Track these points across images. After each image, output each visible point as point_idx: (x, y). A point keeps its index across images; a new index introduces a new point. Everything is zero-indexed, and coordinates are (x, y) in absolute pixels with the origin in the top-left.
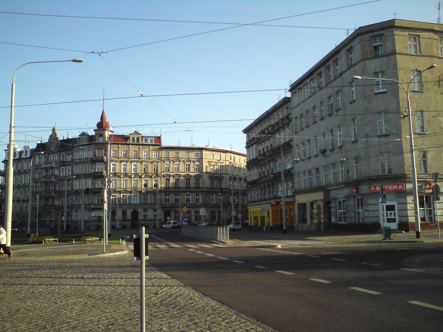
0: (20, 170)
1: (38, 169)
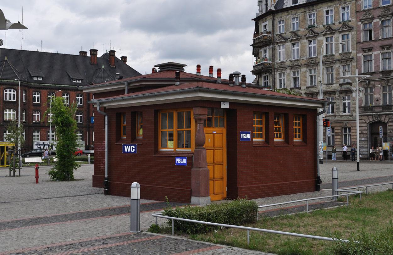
0: (349, 21)
1: (373, 18)
